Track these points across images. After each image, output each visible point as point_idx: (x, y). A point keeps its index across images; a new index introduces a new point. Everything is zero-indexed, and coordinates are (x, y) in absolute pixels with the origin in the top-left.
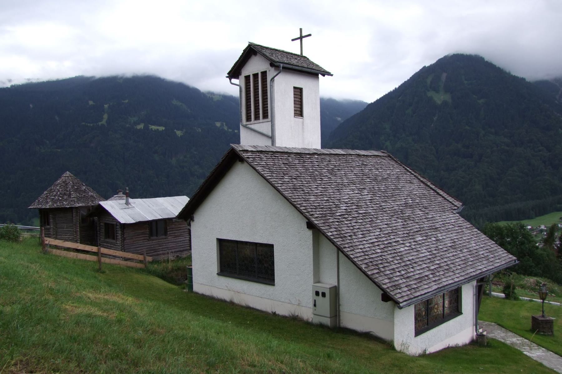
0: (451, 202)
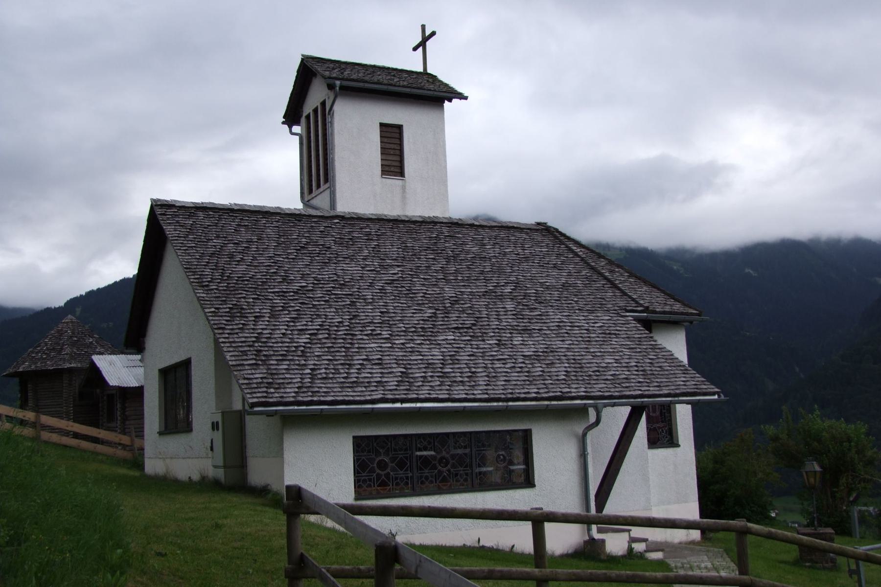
0: (633, 300)
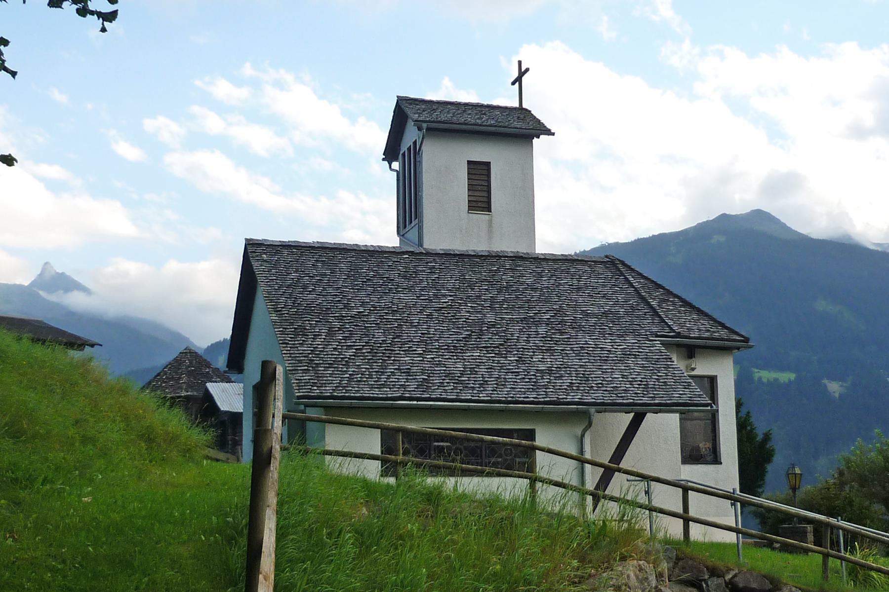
0: (669, 326)
